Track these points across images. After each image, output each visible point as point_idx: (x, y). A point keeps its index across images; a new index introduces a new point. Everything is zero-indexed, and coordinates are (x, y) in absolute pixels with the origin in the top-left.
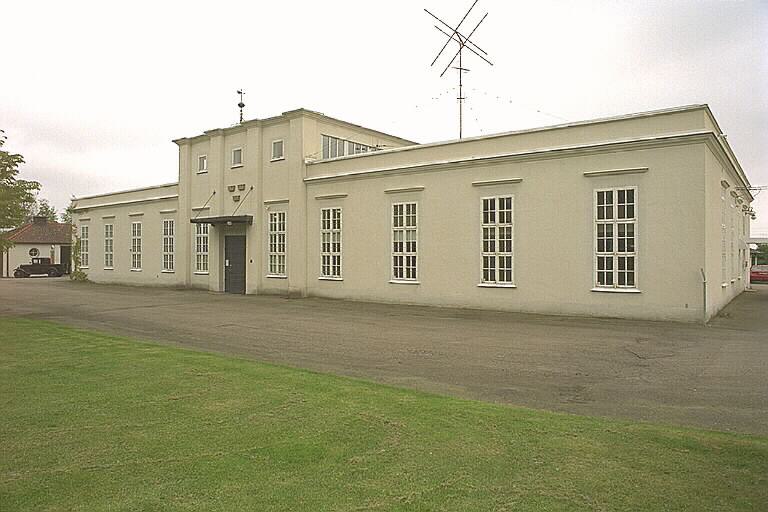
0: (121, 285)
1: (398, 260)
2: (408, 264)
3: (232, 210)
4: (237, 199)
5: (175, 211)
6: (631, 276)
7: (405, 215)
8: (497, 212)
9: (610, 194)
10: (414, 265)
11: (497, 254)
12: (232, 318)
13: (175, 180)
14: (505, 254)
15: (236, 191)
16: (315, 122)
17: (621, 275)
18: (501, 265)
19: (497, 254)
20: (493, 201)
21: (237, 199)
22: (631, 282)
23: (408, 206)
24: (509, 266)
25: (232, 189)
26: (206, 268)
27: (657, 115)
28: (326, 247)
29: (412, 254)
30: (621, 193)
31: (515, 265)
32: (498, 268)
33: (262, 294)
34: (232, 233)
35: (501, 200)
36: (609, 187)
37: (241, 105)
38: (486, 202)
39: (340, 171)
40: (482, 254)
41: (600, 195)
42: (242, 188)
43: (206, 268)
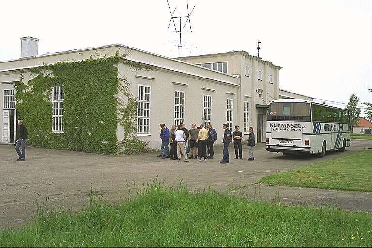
3: (261, 103)
23: (146, 87)
37: (258, 49)
40: (149, 118)
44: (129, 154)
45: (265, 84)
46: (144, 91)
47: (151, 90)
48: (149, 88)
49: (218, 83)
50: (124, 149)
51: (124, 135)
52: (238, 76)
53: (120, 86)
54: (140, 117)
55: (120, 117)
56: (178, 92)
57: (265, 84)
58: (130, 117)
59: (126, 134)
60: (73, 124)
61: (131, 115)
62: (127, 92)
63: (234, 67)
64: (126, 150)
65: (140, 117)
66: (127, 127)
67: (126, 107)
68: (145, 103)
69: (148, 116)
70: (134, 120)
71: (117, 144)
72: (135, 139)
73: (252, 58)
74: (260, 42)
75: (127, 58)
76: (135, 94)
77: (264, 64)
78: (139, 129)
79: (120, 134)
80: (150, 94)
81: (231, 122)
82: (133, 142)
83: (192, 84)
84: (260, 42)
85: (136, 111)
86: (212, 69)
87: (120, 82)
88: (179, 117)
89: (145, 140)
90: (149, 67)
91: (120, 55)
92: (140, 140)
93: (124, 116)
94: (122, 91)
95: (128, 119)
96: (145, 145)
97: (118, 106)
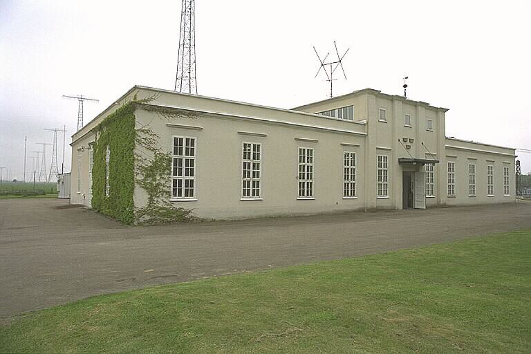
2: (254, 186)
3: (411, 155)
4: (408, 148)
5: (358, 146)
6: (192, 191)
8: (251, 153)
10: (258, 186)
11: (183, 178)
12: (113, 245)
16: (401, 103)
19: (183, 178)
21: (408, 148)
22: (192, 195)
25: (405, 140)
27: (465, 142)
29: (247, 179)
31: (196, 185)
34: (412, 169)
35: (187, 140)
36: (181, 135)
37: (405, 86)
45: (417, 131)
47: (262, 148)
48: (259, 146)
50: (148, 218)
51: (148, 200)
52: (365, 122)
53: (138, 138)
54: (177, 177)
55: (140, 177)
56: (304, 150)
57: (417, 131)
58: (158, 178)
59: (151, 200)
60: (113, 186)
61: (161, 175)
62: (153, 146)
63: (360, 113)
65: (177, 177)
66: (153, 191)
68: (308, 167)
69: (311, 179)
71: (134, 212)
72: (168, 205)
73: (392, 98)
74: (407, 78)
76: (167, 148)
77: (416, 106)
78: (177, 192)
79: (141, 199)
80: (313, 156)
83: (479, 158)
84: (407, 78)
85: (170, 170)
86: (337, 118)
87: (139, 133)
88: (306, 178)
89: (186, 207)
90: (192, 114)
91: (139, 99)
93: (147, 176)
94: (144, 145)
96: (187, 212)
97: (136, 164)
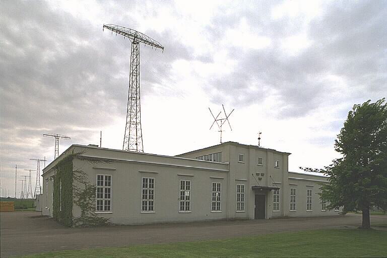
0: (167, 223)
1: (182, 204)
3: (262, 184)
4: (260, 179)
5: (193, 176)
7: (185, 185)
8: (148, 184)
9: (102, 176)
13: (289, 171)
14: (151, 200)
15: (260, 176)
17: (105, 207)
18: (150, 205)
20: (147, 179)
21: (260, 179)
23: (187, 182)
24: (152, 205)
25: (258, 174)
26: (311, 209)
28: (292, 201)
30: (106, 177)
32: (148, 205)
33: (274, 218)
37: (259, 139)
38: (144, 179)
39: (198, 166)
40: (154, 200)
41: (99, 176)
42: (262, 175)
43: (311, 209)
44: (87, 227)
46: (148, 185)
48: (189, 182)
49: (162, 166)
50: (81, 223)
59: (83, 212)
64: (83, 224)
66: (84, 207)
67: (83, 191)
69: (152, 199)
70: (94, 201)
74: (261, 133)
75: (83, 155)
81: (109, 199)
82: (91, 218)
84: (261, 133)
91: (75, 153)
92: (100, 216)
95: (85, 201)
